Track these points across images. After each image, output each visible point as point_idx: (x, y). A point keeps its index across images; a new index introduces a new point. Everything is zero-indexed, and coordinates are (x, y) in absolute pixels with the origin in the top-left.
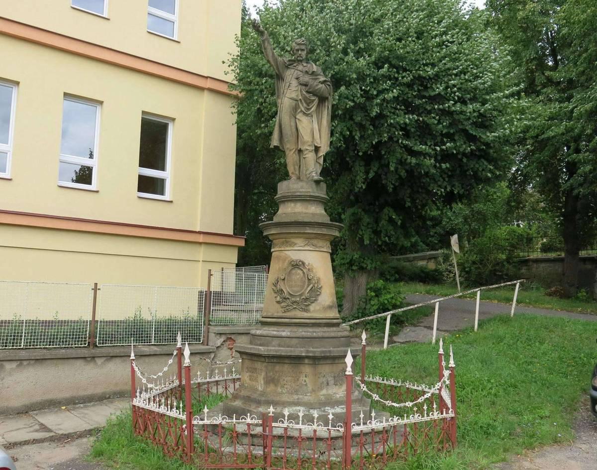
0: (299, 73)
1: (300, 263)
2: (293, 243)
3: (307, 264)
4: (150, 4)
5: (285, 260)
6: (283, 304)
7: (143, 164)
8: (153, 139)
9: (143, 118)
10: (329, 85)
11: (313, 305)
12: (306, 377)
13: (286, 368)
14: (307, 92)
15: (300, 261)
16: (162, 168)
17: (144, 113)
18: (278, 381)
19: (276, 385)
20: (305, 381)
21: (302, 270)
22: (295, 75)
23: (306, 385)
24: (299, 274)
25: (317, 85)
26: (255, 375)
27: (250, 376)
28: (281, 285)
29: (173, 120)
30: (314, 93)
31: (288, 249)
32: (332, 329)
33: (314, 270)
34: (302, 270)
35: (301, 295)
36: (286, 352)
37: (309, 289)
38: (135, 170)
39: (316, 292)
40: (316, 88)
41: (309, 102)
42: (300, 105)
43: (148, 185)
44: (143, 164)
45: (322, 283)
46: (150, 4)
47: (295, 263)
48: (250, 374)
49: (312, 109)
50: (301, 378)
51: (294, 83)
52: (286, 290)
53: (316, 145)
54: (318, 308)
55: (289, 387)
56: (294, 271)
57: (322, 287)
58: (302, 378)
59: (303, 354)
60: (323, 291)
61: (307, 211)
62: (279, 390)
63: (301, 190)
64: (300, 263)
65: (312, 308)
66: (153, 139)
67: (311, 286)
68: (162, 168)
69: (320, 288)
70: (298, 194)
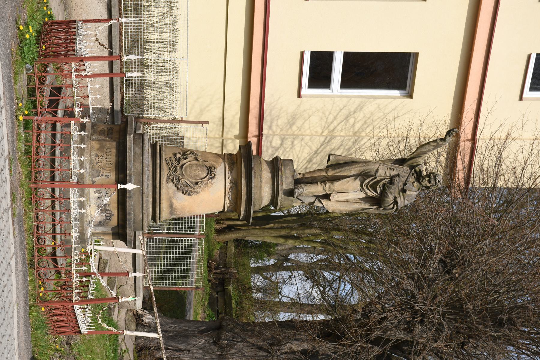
0: (405, 178)
1: (213, 175)
2: (232, 169)
3: (212, 182)
4: (538, 55)
5: (215, 162)
6: (173, 159)
7: (348, 57)
8: (384, 71)
9: (410, 53)
10: (393, 208)
11: (174, 186)
12: (106, 176)
13: (113, 159)
14: (384, 185)
15: (215, 175)
16: (346, 84)
17: (416, 55)
18: (102, 151)
19: (98, 149)
20: (102, 175)
21: (206, 177)
22: (402, 174)
23: (99, 176)
24: (202, 174)
25: (391, 194)
26: (106, 134)
27: (104, 130)
28: (191, 158)
29: (410, 96)
30: (383, 194)
31: (228, 181)
32: (151, 206)
33: (206, 189)
34: (206, 177)
35: (182, 174)
36: (129, 157)
37: (189, 183)
38: (340, 45)
39: (186, 190)
40: (388, 193)
41: (374, 187)
42: (371, 179)
43: (319, 69)
44: (348, 57)
45: (194, 196)
46: (538, 55)
47: (213, 170)
48: (107, 131)
49: (368, 191)
50: (105, 171)
51: (394, 173)
52: (187, 162)
53: (332, 195)
54: (171, 191)
55: (97, 161)
56: (205, 169)
57: (191, 195)
58: (105, 173)
59: (128, 172)
60: (186, 197)
61: (264, 182)
62: (94, 153)
63: (284, 176)
64: (213, 175)
65: (171, 185)
66: (384, 71)
67: (191, 185)
68: (346, 84)
69: (189, 194)
70: (280, 174)
